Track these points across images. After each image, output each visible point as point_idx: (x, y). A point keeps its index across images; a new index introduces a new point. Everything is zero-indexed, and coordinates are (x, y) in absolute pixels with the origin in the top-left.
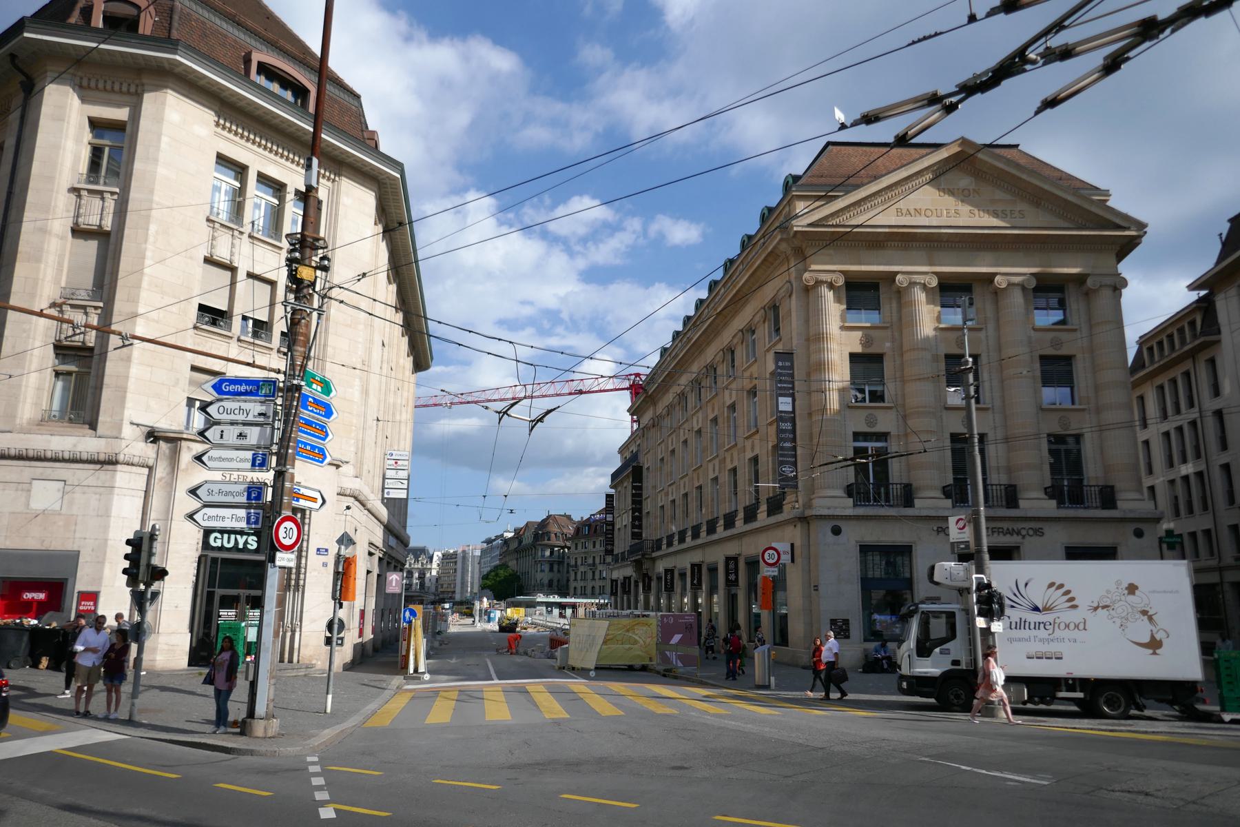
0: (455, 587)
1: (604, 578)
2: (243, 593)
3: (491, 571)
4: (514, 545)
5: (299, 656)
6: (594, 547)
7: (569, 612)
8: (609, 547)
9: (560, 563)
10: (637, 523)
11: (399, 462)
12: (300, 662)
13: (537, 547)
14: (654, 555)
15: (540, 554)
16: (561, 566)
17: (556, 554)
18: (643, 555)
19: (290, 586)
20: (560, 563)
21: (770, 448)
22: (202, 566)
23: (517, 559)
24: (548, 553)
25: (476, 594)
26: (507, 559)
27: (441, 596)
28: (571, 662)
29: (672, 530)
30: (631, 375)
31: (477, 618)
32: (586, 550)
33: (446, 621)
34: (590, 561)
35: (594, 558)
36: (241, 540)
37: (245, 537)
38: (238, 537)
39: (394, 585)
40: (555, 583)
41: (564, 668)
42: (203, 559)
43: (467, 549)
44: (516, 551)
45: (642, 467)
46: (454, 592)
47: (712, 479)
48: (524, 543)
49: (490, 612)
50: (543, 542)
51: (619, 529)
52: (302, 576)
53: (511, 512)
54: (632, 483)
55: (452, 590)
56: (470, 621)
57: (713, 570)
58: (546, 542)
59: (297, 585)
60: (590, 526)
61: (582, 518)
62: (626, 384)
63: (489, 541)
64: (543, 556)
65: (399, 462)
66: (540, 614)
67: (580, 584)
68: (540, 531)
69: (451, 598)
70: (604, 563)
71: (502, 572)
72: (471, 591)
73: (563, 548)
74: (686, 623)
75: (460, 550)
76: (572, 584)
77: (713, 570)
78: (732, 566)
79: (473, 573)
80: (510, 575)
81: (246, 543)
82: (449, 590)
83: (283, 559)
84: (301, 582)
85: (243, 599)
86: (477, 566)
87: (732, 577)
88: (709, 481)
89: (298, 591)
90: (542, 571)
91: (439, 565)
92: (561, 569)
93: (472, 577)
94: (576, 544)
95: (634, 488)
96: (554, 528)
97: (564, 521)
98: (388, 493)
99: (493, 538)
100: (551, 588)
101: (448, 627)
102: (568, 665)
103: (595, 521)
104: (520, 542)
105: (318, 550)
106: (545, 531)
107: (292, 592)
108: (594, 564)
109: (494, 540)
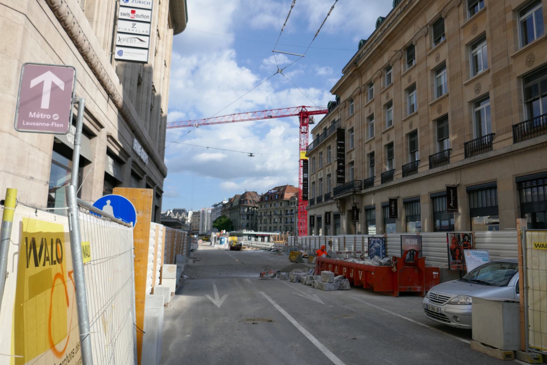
0: (199, 228)
1: (276, 222)
3: (217, 219)
4: (229, 206)
6: (271, 206)
7: (260, 239)
9: (252, 215)
10: (341, 171)
11: (138, 12)
13: (241, 207)
14: (363, 191)
15: (242, 210)
16: (253, 217)
17: (250, 210)
18: (354, 192)
20: (252, 215)
21: (404, 135)
23: (230, 213)
24: (246, 210)
25: (209, 231)
26: (225, 213)
27: (192, 232)
29: (385, 169)
30: (300, 107)
31: (213, 242)
32: (267, 208)
33: (197, 243)
34: (269, 214)
35: (271, 212)
39: (45, 103)
40: (250, 225)
43: (204, 209)
44: (230, 209)
45: (344, 130)
46: (198, 230)
47: (470, 102)
48: (234, 205)
49: (221, 239)
50: (244, 205)
51: (314, 183)
54: (338, 140)
55: (198, 229)
56: (209, 243)
57: (319, 219)
58: (245, 204)
60: (268, 196)
61: (262, 194)
62: (298, 112)
63: (215, 206)
64: (244, 211)
65: (138, 12)
66: (245, 240)
67: (263, 225)
68: (242, 199)
69: (197, 233)
72: (207, 230)
73: (254, 207)
75: (201, 210)
76: (259, 226)
77: (319, 219)
79: (207, 221)
80: (227, 221)
82: (196, 229)
83: (156, 230)
86: (209, 218)
88: (466, 105)
90: (243, 219)
91: (191, 217)
92: (253, 218)
93: (207, 223)
94: (261, 205)
95: (339, 145)
96: (249, 198)
97: (254, 195)
98: (120, 53)
99: (218, 204)
100: (248, 228)
101: (197, 247)
103: (271, 193)
104: (232, 205)
106: (245, 199)
108: (271, 215)
109: (218, 205)
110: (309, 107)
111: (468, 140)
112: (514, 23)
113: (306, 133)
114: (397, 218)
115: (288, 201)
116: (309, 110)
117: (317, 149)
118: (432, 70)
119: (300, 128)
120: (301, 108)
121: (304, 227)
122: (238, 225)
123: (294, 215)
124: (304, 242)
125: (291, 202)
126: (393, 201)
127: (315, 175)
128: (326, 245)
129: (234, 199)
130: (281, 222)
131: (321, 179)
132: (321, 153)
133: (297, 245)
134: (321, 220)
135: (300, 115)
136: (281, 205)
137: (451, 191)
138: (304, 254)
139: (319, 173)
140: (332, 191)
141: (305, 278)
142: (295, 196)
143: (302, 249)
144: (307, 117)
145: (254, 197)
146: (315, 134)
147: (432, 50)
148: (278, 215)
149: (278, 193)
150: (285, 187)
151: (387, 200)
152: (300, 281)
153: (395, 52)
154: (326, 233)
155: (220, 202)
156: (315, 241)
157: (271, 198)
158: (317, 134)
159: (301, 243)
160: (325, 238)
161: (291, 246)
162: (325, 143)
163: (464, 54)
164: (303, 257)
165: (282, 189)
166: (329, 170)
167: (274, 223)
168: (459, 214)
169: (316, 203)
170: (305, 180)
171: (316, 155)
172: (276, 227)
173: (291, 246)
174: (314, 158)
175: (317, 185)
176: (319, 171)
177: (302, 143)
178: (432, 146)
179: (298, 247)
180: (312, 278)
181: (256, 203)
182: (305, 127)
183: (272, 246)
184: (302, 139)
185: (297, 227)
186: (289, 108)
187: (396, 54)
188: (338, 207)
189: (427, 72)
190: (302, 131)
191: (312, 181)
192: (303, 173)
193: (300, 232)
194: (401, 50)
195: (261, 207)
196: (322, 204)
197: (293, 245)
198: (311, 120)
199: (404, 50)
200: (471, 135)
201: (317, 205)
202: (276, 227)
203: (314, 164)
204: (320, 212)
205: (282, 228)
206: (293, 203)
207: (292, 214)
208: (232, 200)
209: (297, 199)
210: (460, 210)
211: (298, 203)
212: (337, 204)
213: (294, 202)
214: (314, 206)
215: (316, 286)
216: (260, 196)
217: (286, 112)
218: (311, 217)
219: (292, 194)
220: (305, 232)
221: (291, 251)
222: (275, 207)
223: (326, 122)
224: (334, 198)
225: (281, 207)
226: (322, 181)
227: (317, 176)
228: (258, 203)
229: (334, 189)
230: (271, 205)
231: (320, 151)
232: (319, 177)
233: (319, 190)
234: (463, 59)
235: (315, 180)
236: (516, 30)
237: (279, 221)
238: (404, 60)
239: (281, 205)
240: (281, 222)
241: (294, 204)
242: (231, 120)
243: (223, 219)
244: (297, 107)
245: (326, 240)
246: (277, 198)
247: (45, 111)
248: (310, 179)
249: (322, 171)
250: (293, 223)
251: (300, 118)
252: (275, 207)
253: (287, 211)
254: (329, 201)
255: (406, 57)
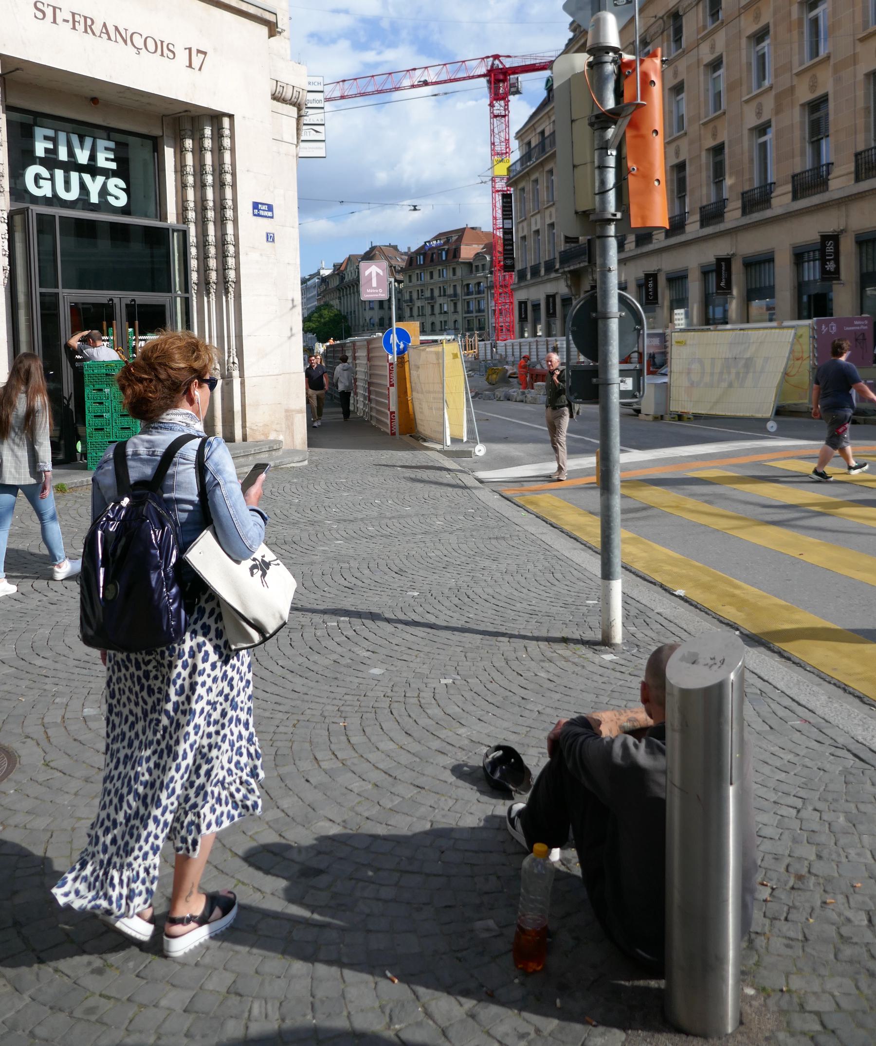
1: (445, 312)
2: (121, 298)
4: (335, 283)
5: (244, 426)
6: (432, 277)
8: (509, 262)
12: (249, 439)
19: (208, 283)
22: (18, 237)
23: (340, 298)
28: (676, 407)
30: (488, 57)
34: (428, 294)
35: (432, 290)
36: (94, 186)
37: (100, 179)
38: (87, 177)
39: (374, 284)
41: (662, 417)
42: (18, 219)
44: (338, 289)
47: (751, 130)
48: (346, 279)
51: (524, 238)
52: (231, 262)
53: (415, 209)
57: (536, 307)
59: (224, 281)
60: (425, 254)
61: (409, 248)
62: (483, 70)
70: (445, 295)
71: (326, 312)
74: (855, 332)
77: (536, 307)
78: (830, 249)
80: (336, 315)
81: (104, 192)
84: (232, 274)
85: (120, 313)
87: (831, 266)
88: (746, 133)
89: (227, 292)
94: (410, 277)
97: (390, 252)
102: (671, 413)
103: (431, 248)
105: (256, 205)
107: (213, 296)
108: (432, 297)
110: (509, 56)
111: (747, 188)
112: (800, 21)
113: (504, 116)
114: (657, 303)
115: (469, 264)
116: (508, 63)
117: (528, 174)
118: (706, 66)
119: (491, 105)
120: (491, 59)
121: (508, 319)
122: (361, 323)
123: (485, 295)
124: (510, 351)
125: (477, 267)
126: (651, 277)
127: (525, 224)
128: (530, 352)
129: (347, 264)
130: (455, 312)
131: (537, 232)
132: (536, 181)
133: (498, 357)
134: (540, 309)
135: (490, 76)
136: (454, 274)
137: (723, 264)
138: (510, 372)
139: (533, 220)
140: (557, 256)
141: (515, 394)
142: (485, 253)
143: (507, 363)
144: (504, 81)
145: (391, 258)
146: (522, 140)
147: (706, 32)
148: (450, 296)
149: (446, 247)
150: (461, 232)
151: (642, 275)
152: (509, 400)
153: (653, 20)
154: (549, 333)
155: (315, 271)
156: (530, 349)
157: (432, 260)
158: (526, 140)
159: (503, 353)
160: (547, 341)
161: (485, 360)
162: (542, 164)
163: (745, 54)
164: (510, 377)
165: (454, 238)
166: (551, 216)
167: (441, 313)
168: (733, 298)
169: (529, 276)
170: (508, 232)
171: (527, 185)
172: (445, 322)
173: (485, 360)
174: (523, 189)
175: (531, 242)
176: (532, 216)
177: (497, 141)
178: (704, 191)
179: (500, 361)
180: (523, 393)
181: (398, 272)
182: (502, 103)
183: (84, 444)
184: (496, 131)
185: (492, 320)
186: (464, 62)
187: (655, 22)
188: (567, 286)
189: (698, 67)
190: (496, 112)
191: (521, 235)
192: (504, 219)
193: (498, 330)
194: (662, 18)
195: (410, 281)
196: (540, 279)
197: (489, 357)
198: (513, 85)
199: (668, 17)
200: (751, 180)
201: (532, 281)
202: (445, 322)
203: (522, 200)
204: (537, 293)
205: (460, 325)
206: (480, 267)
207: (479, 292)
208: (342, 268)
209: (488, 259)
210: (735, 292)
211: (491, 267)
212: (566, 280)
213: (483, 265)
214: (527, 283)
215: (528, 400)
216: (406, 254)
217: (458, 70)
218: (520, 303)
219: (477, 248)
220: (510, 330)
221: (487, 368)
222: (441, 279)
223: (542, 121)
224: (561, 271)
225: (455, 278)
226: (539, 235)
227: (530, 225)
228: (402, 271)
229: (560, 253)
230: (431, 274)
231: (533, 177)
232: (534, 228)
233: (535, 252)
234: (744, 60)
235: (525, 233)
236: (803, 33)
237: (452, 309)
238: (669, 36)
239: (454, 274)
240: (455, 312)
241: (484, 269)
242: (337, 94)
243: (325, 312)
244: (483, 59)
245: (547, 345)
246: (444, 258)
247: (375, 288)
248: (517, 231)
249: (538, 217)
250: (483, 311)
251: (489, 82)
252: (441, 279)
253: (468, 285)
254: (553, 275)
255: (671, 31)
